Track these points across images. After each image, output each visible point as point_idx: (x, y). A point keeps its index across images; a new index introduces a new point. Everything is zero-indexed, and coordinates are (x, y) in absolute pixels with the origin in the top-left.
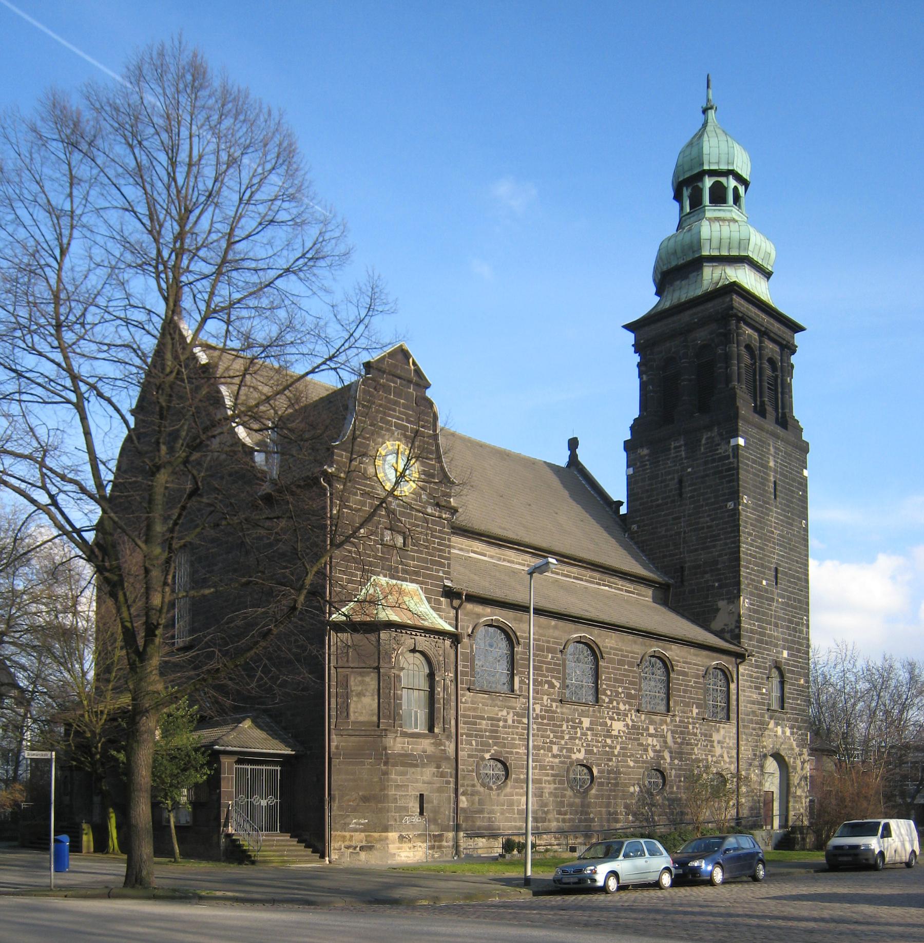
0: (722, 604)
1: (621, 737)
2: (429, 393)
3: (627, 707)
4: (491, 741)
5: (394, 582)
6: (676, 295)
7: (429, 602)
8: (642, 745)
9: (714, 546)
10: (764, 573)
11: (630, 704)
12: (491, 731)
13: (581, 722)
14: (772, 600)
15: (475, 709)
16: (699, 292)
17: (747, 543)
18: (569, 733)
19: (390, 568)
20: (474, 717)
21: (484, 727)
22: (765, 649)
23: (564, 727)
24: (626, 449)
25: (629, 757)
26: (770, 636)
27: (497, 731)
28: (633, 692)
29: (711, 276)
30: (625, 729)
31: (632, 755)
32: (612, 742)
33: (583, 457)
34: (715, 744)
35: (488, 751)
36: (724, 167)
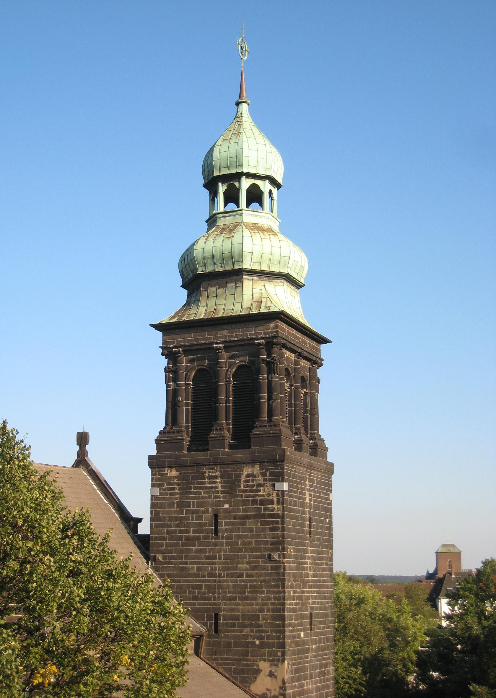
0: (264, 666)
6: (212, 302)
9: (255, 599)
16: (237, 310)
29: (251, 296)
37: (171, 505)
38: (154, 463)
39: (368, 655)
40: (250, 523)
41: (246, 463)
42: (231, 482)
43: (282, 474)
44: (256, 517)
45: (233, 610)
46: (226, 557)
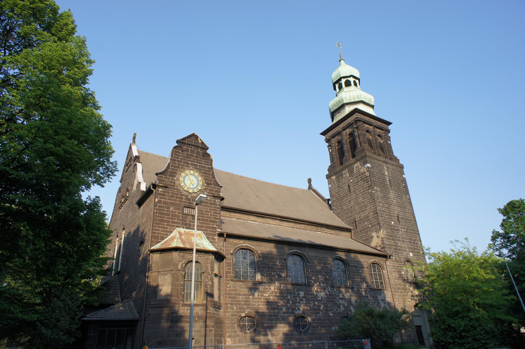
0: (374, 234)
1: (323, 301)
2: (208, 151)
3: (325, 285)
4: (245, 307)
5: (188, 230)
7: (208, 239)
8: (336, 304)
9: (366, 210)
10: (391, 219)
11: (326, 283)
12: (245, 301)
13: (299, 294)
14: (399, 230)
15: (235, 290)
17: (380, 206)
18: (292, 300)
19: (186, 224)
20: (235, 294)
21: (241, 299)
22: (399, 253)
23: (289, 297)
24: (327, 178)
25: (330, 311)
26: (400, 247)
27: (249, 301)
28: (327, 277)
30: (325, 296)
31: (331, 310)
32: (319, 303)
33: (314, 186)
34: (380, 301)
35: (244, 312)
36: (348, 75)
37: (335, 188)
38: (328, 177)
39: (177, 306)
40: (360, 183)
41: (354, 163)
42: (351, 172)
43: (367, 161)
44: (361, 180)
45: (360, 217)
46: (354, 199)
